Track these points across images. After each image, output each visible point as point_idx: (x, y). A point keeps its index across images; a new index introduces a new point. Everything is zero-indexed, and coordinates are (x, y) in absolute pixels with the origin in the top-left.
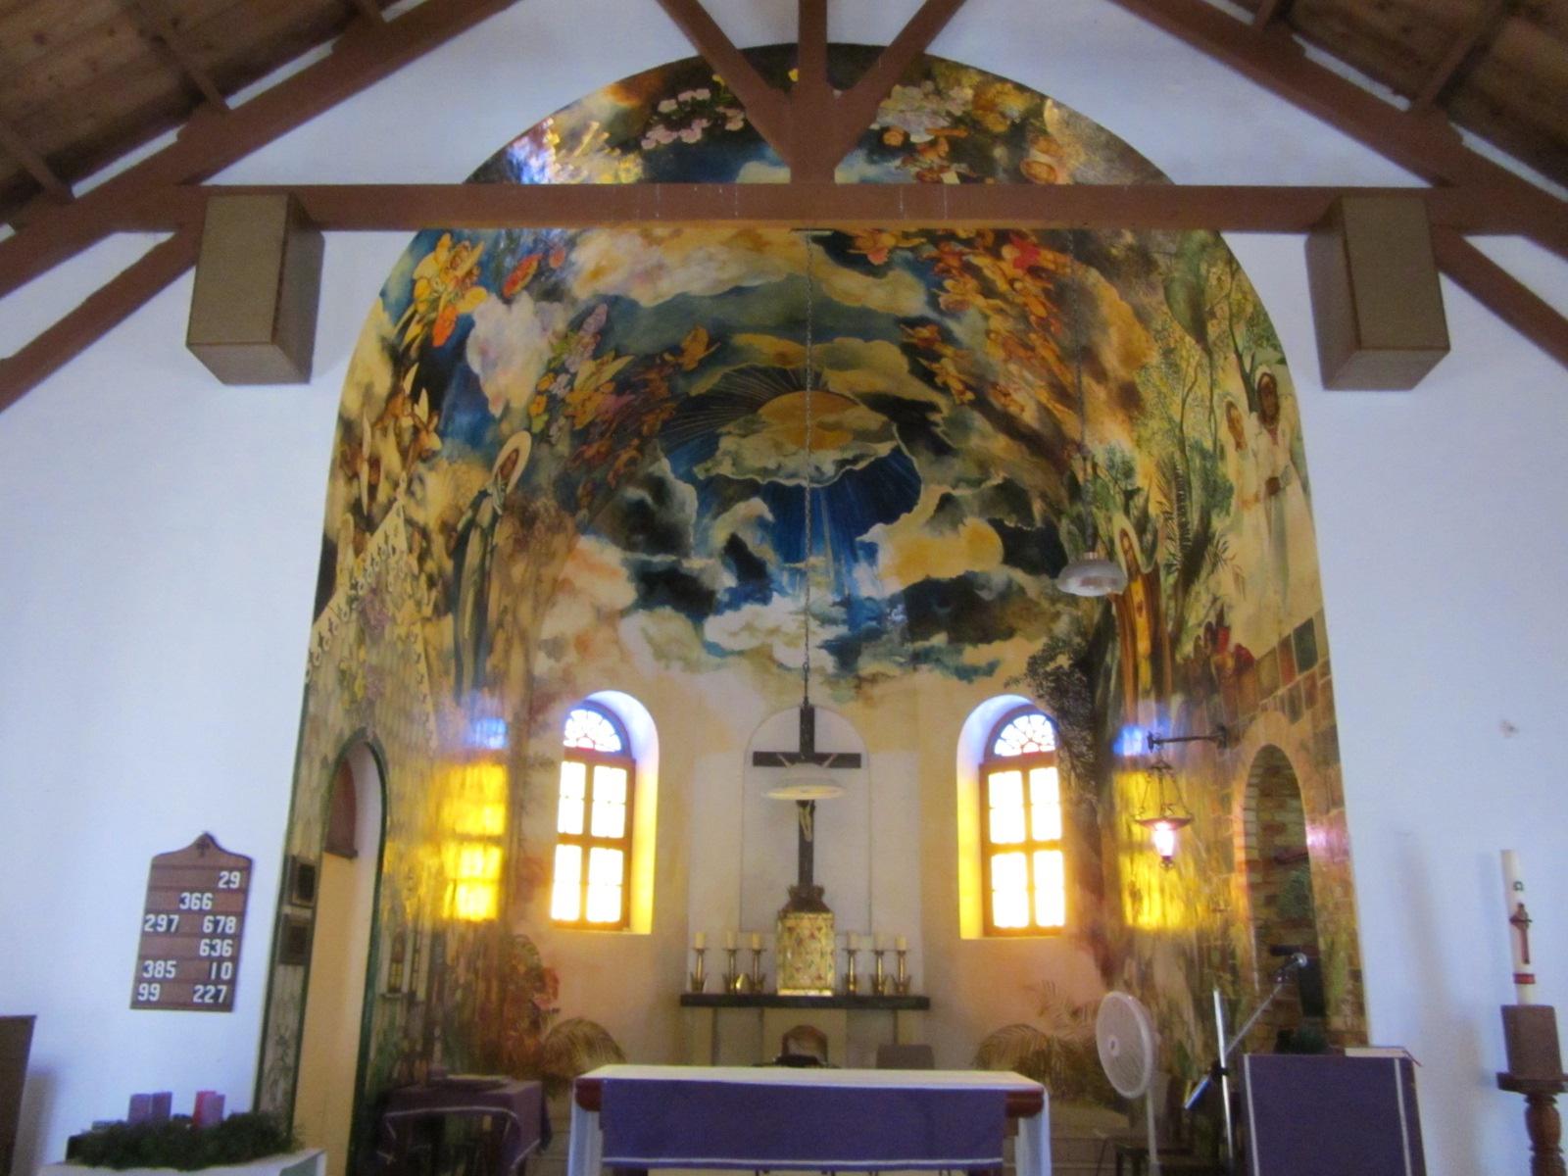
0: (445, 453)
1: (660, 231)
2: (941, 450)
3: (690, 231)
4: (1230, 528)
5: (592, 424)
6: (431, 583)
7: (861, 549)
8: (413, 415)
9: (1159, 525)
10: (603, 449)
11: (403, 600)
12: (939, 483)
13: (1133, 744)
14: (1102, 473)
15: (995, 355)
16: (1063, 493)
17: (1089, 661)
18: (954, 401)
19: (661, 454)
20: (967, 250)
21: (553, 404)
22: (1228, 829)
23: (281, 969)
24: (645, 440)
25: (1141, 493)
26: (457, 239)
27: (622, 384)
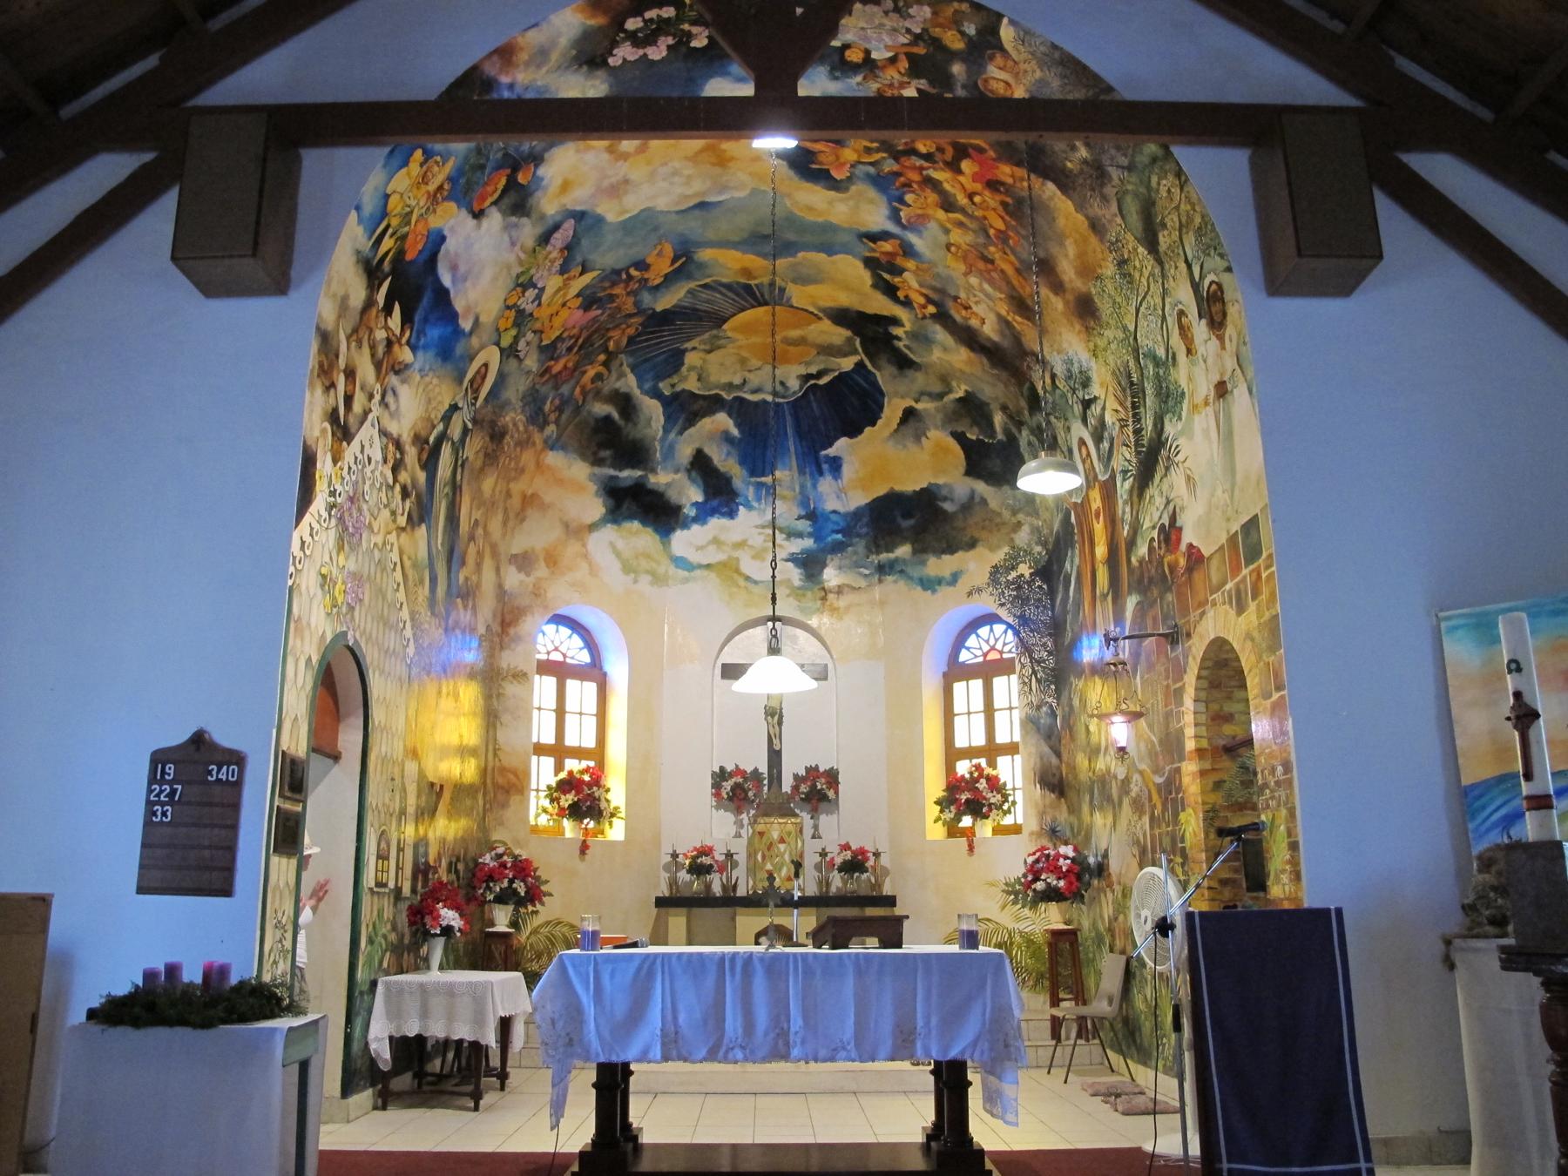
0: (417, 366)
1: (628, 145)
2: (904, 363)
3: (657, 145)
4: (1182, 433)
5: (559, 338)
6: (405, 494)
7: (826, 462)
8: (387, 328)
9: (1115, 434)
10: (570, 365)
11: (379, 509)
12: (902, 397)
13: (1091, 651)
14: (1061, 384)
15: (955, 268)
16: (1023, 403)
17: (1049, 572)
18: (916, 315)
19: (628, 370)
20: (926, 164)
21: (521, 318)
22: (1179, 722)
23: (275, 859)
24: (611, 356)
25: (1098, 401)
26: (428, 155)
27: (589, 300)
